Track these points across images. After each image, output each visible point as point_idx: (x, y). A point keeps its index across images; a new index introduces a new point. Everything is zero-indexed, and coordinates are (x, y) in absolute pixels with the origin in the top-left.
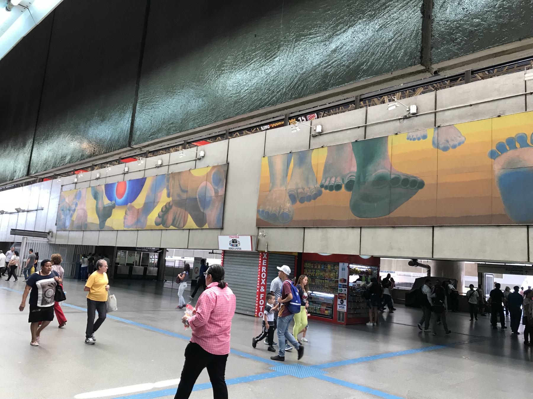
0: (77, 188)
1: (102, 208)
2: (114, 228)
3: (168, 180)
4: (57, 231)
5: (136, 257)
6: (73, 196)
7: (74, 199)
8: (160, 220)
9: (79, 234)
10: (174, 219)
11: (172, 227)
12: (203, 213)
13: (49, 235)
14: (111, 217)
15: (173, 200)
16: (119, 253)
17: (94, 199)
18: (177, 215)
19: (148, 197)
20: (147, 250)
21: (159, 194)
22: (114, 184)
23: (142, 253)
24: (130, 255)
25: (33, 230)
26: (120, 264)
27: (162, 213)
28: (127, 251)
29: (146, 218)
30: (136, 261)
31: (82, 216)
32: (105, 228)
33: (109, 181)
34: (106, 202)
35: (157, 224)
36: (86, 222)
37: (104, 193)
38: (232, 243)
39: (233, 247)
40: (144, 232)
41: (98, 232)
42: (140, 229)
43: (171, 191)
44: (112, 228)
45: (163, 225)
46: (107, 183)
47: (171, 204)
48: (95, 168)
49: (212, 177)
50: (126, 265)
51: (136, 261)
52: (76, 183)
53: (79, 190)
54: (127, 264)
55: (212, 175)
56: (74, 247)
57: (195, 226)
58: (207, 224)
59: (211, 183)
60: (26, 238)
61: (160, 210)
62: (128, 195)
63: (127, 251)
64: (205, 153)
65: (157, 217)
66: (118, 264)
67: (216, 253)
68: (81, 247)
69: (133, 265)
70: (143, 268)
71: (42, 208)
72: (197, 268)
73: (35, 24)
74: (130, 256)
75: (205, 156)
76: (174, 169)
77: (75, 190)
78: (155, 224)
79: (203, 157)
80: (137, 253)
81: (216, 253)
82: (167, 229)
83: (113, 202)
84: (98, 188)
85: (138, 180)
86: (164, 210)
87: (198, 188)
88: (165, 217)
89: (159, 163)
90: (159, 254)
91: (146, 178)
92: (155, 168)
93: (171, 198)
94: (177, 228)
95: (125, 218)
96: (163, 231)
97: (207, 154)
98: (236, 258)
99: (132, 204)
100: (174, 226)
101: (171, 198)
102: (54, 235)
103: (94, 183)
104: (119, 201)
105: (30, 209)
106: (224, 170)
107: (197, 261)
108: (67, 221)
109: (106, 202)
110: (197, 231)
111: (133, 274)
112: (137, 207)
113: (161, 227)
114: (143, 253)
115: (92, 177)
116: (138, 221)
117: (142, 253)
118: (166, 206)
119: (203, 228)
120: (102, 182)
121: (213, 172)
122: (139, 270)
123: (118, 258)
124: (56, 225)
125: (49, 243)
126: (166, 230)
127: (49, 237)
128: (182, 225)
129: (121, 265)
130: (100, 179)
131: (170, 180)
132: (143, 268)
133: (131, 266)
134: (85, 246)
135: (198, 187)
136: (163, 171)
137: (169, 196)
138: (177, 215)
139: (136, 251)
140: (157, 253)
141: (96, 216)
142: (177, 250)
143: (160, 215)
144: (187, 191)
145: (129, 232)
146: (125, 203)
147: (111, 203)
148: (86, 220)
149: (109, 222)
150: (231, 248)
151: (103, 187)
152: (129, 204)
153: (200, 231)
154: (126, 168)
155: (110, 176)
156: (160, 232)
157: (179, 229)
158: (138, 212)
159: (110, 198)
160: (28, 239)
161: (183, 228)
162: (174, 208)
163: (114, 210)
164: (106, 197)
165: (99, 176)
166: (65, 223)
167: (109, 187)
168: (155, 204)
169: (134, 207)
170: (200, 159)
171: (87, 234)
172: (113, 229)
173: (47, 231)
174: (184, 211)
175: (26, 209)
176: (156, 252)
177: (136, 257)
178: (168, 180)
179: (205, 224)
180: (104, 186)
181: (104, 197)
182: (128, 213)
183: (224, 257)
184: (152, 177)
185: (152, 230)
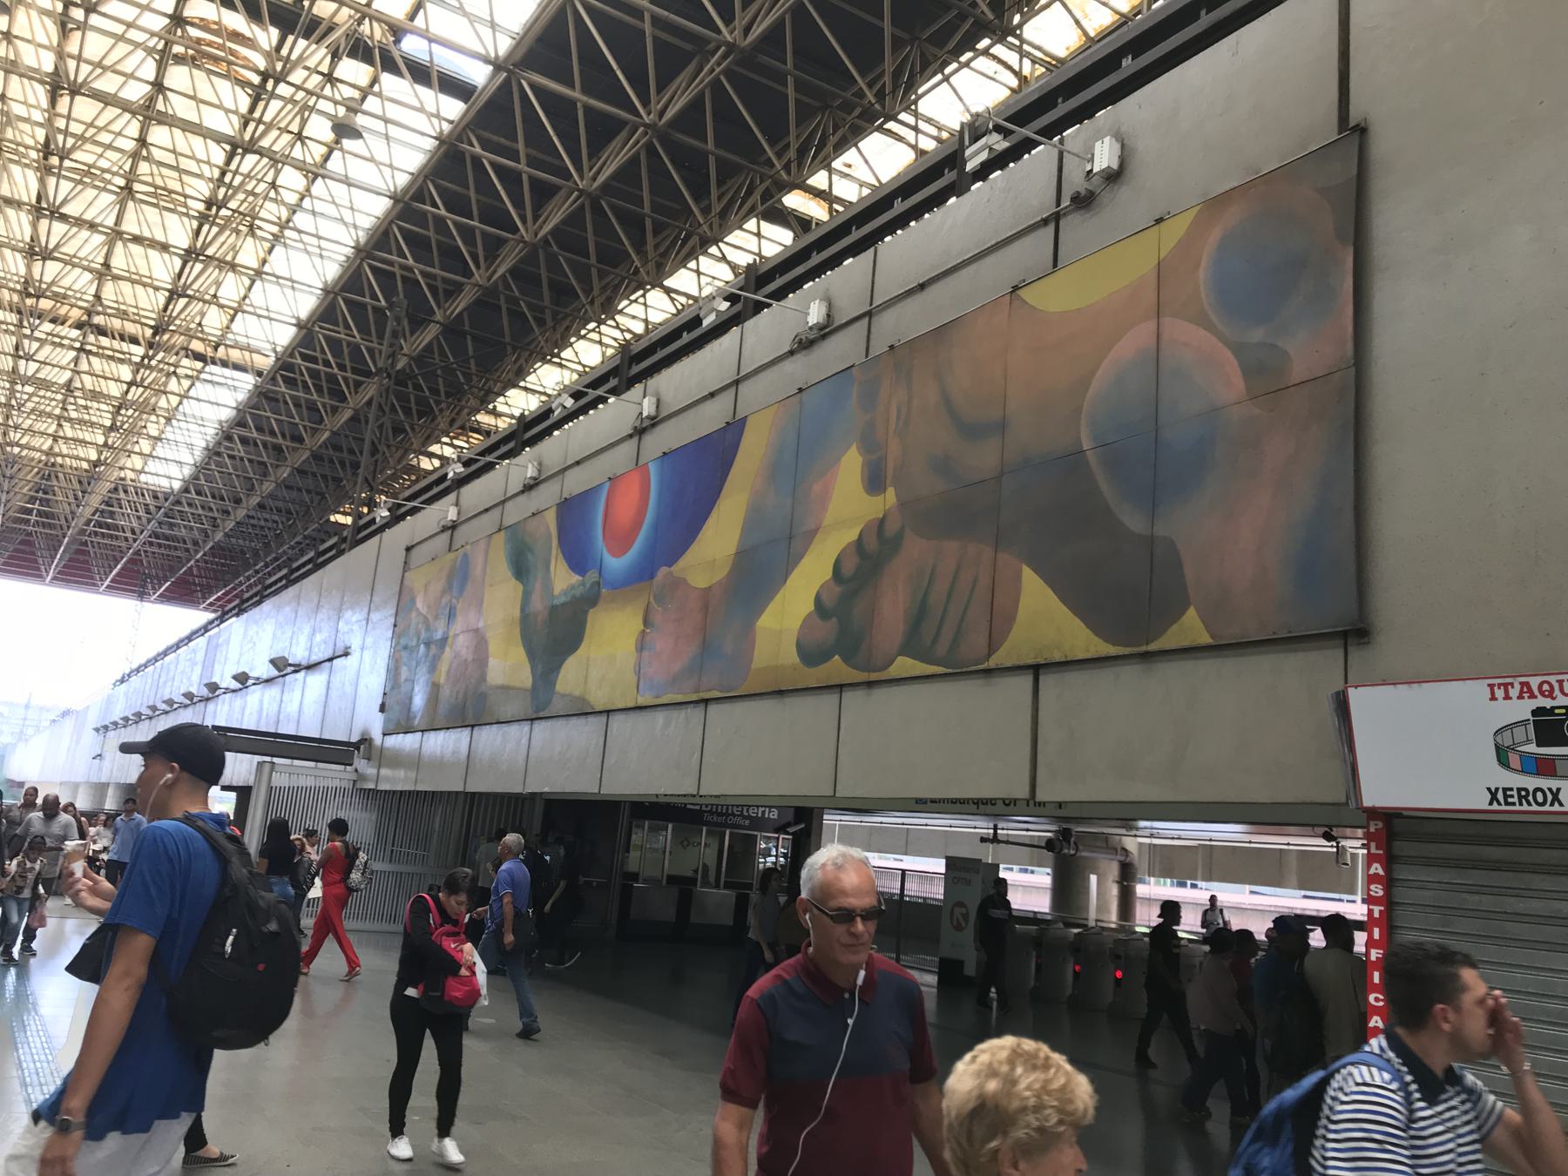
4: (384, 735)
5: (706, 851)
7: (443, 593)
8: (827, 631)
10: (918, 618)
11: (905, 665)
13: (359, 751)
15: (902, 504)
16: (636, 838)
20: (747, 822)
21: (817, 488)
23: (728, 832)
24: (682, 841)
27: (838, 589)
29: (748, 631)
31: (470, 658)
32: (557, 706)
33: (575, 483)
34: (563, 580)
35: (811, 654)
37: (555, 542)
38: (1532, 748)
40: (739, 708)
42: (717, 694)
43: (894, 450)
45: (846, 659)
47: (891, 528)
48: (490, 387)
49: (1202, 274)
50: (664, 882)
52: (453, 527)
54: (673, 880)
57: (1080, 639)
59: (1203, 321)
60: (267, 768)
62: (656, 527)
63: (670, 826)
65: (809, 615)
66: (635, 877)
67: (1007, 842)
68: (401, 795)
69: (693, 881)
70: (730, 895)
72: (960, 904)
73: (687, 787)
74: (682, 842)
77: (452, 556)
78: (797, 660)
79: (1113, 177)
80: (708, 833)
81: (1007, 842)
82: (874, 676)
83: (592, 576)
86: (849, 569)
89: (815, 314)
90: (793, 840)
91: (744, 420)
93: (891, 492)
94: (951, 671)
95: (641, 646)
96: (848, 696)
100: (922, 660)
101: (891, 492)
102: (375, 754)
103: (515, 512)
104: (615, 564)
109: (563, 580)
110: (1104, 677)
111: (694, 918)
112: (700, 580)
113: (836, 668)
114: (731, 834)
115: (509, 489)
116: (707, 649)
117: (728, 832)
118: (859, 543)
119: (1153, 647)
120: (547, 496)
121: (1215, 236)
122: (716, 901)
123: (634, 855)
124: (382, 709)
125: (358, 786)
126: (870, 684)
128: (979, 640)
129: (645, 881)
130: (542, 487)
132: (730, 895)
133: (683, 886)
135: (1093, 373)
136: (841, 351)
137: (874, 482)
139: (707, 824)
140: (788, 833)
141: (519, 654)
143: (828, 602)
146: (644, 572)
147: (583, 584)
149: (571, 677)
150: (1523, 795)
152: (664, 570)
153: (1130, 672)
154: (646, 401)
156: (831, 699)
157: (960, 670)
158: (706, 607)
159: (578, 560)
160: (277, 768)
161: (992, 663)
162: (915, 548)
165: (535, 474)
167: (573, 511)
169: (684, 581)
170: (1084, 201)
171: (489, 737)
172: (588, 704)
173: (354, 739)
176: (781, 829)
177: (706, 851)
182: (657, 618)
183: (1387, 869)
185: (780, 693)
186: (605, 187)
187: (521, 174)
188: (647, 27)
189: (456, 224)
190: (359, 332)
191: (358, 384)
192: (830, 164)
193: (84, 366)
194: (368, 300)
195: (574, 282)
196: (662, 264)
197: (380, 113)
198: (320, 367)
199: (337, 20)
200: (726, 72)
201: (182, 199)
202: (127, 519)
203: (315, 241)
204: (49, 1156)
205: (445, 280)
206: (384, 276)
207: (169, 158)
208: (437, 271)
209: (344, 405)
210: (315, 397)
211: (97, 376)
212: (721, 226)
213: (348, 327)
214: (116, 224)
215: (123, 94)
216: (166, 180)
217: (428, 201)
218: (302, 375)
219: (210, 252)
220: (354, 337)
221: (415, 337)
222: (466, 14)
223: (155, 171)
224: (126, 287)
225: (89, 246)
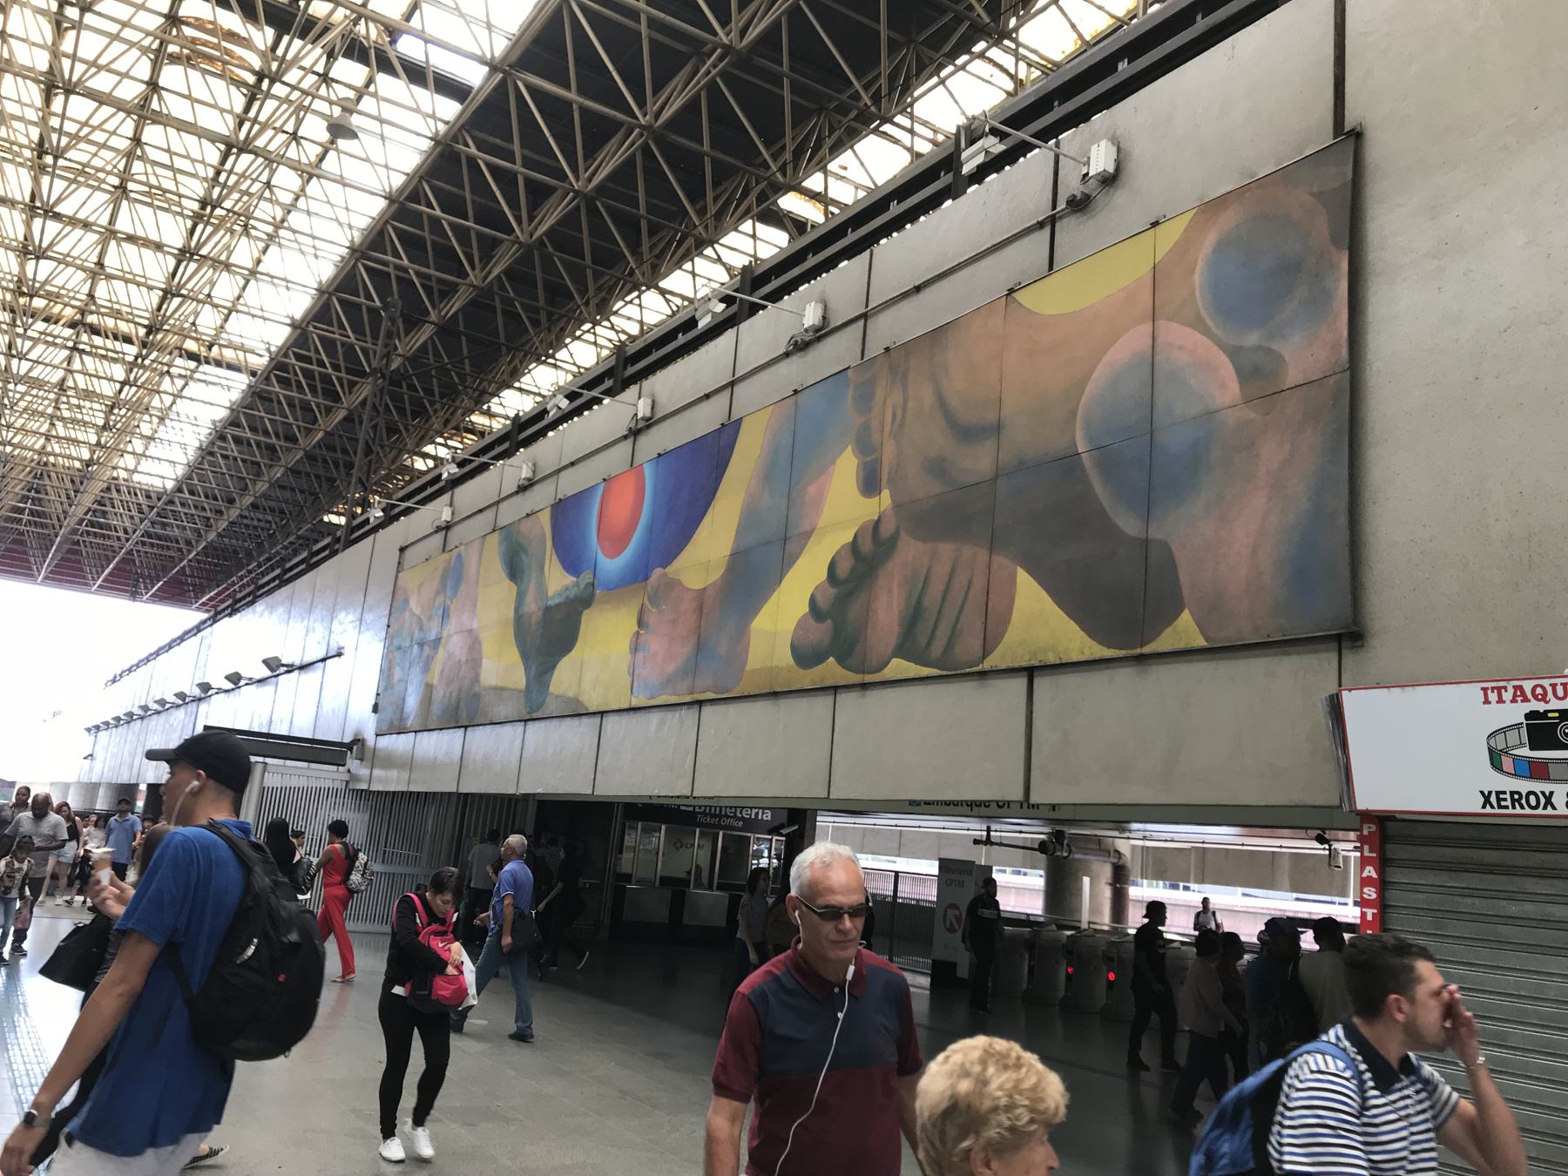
0: (451, 544)
1: (540, 614)
2: (586, 703)
3: (865, 399)
4: (377, 735)
5: (700, 852)
6: (434, 584)
7: (438, 593)
8: (821, 632)
9: (439, 746)
10: (913, 618)
11: (899, 667)
12: (1146, 543)
14: (573, 653)
15: (897, 506)
16: (629, 840)
17: (508, 580)
18: (935, 590)
19: (750, 518)
22: (590, 491)
24: (676, 843)
25: (309, 736)
26: (633, 881)
27: (832, 591)
28: (640, 824)
30: (697, 866)
31: (464, 659)
32: (551, 707)
34: (557, 581)
35: (805, 656)
36: (477, 689)
38: (1525, 752)
39: (1546, 787)
40: (733, 710)
41: (519, 727)
43: (889, 452)
44: (577, 701)
45: (841, 661)
46: (560, 496)
47: (886, 530)
49: (1197, 278)
50: (657, 883)
51: (697, 866)
52: (448, 527)
53: (455, 552)
54: (665, 881)
55: (1200, 265)
56: (453, 804)
57: (1075, 641)
58: (1186, 617)
59: (1198, 324)
61: (823, 575)
62: (650, 529)
64: (1119, 150)
65: (804, 617)
66: (628, 878)
71: (339, 648)
72: (953, 906)
75: (1123, 177)
76: (893, 328)
78: (791, 661)
79: (1109, 180)
80: (701, 833)
81: (1001, 844)
82: (869, 678)
83: (586, 577)
84: (525, 527)
85: (695, 446)
86: (843, 570)
87: (1081, 385)
88: (854, 610)
89: (811, 316)
92: (787, 355)
93: (886, 494)
96: (843, 698)
97: (1133, 171)
98: (1530, 885)
99: (670, 569)
101: (886, 494)
102: (368, 755)
103: (510, 513)
104: (611, 565)
105: (308, 659)
106: (1318, 195)
107: (954, 876)
108: (410, 690)
109: (557, 581)
111: (687, 919)
113: (831, 670)
114: (724, 834)
118: (854, 546)
119: (1147, 649)
120: (542, 497)
123: (627, 856)
124: (375, 709)
126: (864, 686)
127: (352, 763)
129: (638, 882)
130: (536, 488)
131: (879, 394)
133: (676, 887)
134: (442, 793)
136: (837, 352)
137: (870, 485)
138: (935, 590)
140: (781, 835)
141: (513, 655)
142: (838, 828)
143: (823, 603)
144: (997, 429)
145: (654, 718)
146: (638, 574)
148: (476, 680)
149: (565, 678)
150: (1516, 798)
151: (545, 519)
152: (658, 571)
153: (1124, 675)
155: (573, 464)
156: (824, 702)
157: (954, 672)
159: (572, 563)
160: (269, 768)
161: (987, 665)
162: (910, 551)
163: (586, 615)
164: (555, 557)
165: (530, 475)
166: (404, 699)
167: (566, 512)
168: (790, 547)
170: (1079, 205)
173: (347, 740)
174: (983, 555)
175: (297, 663)
177: (700, 852)
178: (865, 399)
179: (1177, 615)
180: (548, 510)
181: (548, 557)
182: (652, 617)
184: (766, 413)
185: (775, 695)
186: (601, 188)
188: (644, 29)
189: (451, 224)
190: (353, 332)
191: (352, 384)
193: (77, 365)
202: (119, 519)
203: (309, 241)
206: (378, 276)
208: (431, 272)
210: (309, 397)
211: (90, 375)
213: (341, 326)
214: (110, 224)
218: (296, 374)
219: (204, 252)
220: (349, 337)
222: (462, 15)
224: (129, 248)
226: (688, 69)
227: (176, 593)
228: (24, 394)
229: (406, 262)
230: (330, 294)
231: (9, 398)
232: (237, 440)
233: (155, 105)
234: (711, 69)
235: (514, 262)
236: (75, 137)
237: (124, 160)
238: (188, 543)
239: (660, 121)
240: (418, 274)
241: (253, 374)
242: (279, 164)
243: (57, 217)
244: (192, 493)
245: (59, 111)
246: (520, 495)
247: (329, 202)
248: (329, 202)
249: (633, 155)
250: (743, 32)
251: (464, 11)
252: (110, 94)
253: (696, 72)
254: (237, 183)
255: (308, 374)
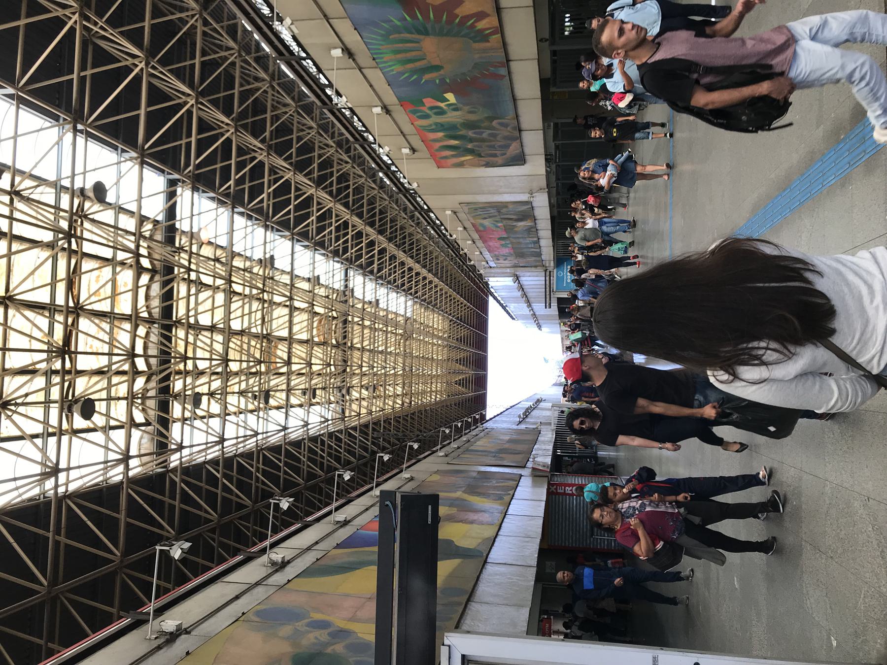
98: (534, 286)
186: (191, 86)
187: (238, 162)
188: (89, 72)
189: (236, 174)
190: (309, 218)
191: (353, 226)
192: (610, 359)
193: (359, 346)
194: (292, 216)
195: (250, 101)
196: (227, 47)
197: (189, 220)
198: (333, 236)
199: (146, 246)
200: (101, 16)
201: (265, 310)
202: (463, 333)
203: (268, 245)
204: (546, 547)
205: (270, 175)
206: (277, 208)
207: (246, 318)
208: (266, 180)
209: (350, 222)
210: (363, 244)
211: (363, 338)
212: (192, 10)
213: (308, 225)
214: (286, 340)
215: (183, 338)
216: (257, 319)
217: (228, 191)
218: (339, 245)
219: (288, 294)
220: (313, 220)
221: (278, 171)
222: (118, 181)
223: (254, 325)
224: (296, 329)
225: (300, 351)
226: (103, 44)
227: (483, 307)
228: (378, 363)
229: (264, 195)
230: (293, 234)
231: (378, 371)
232: (379, 270)
233: (221, 326)
234: (99, 26)
235: (247, 131)
236: (249, 355)
237: (203, 333)
238: (465, 306)
239: (191, 93)
240: (269, 188)
241: (172, 183)
242: (232, 266)
243: (289, 358)
244: (411, 288)
245: (770, 346)
246: (355, 57)
247: (245, 237)
248: (245, 237)
249: (170, 71)
250: (134, 56)
251: (116, 181)
252: (223, 344)
253: (104, 38)
254: (248, 282)
255: (337, 239)
